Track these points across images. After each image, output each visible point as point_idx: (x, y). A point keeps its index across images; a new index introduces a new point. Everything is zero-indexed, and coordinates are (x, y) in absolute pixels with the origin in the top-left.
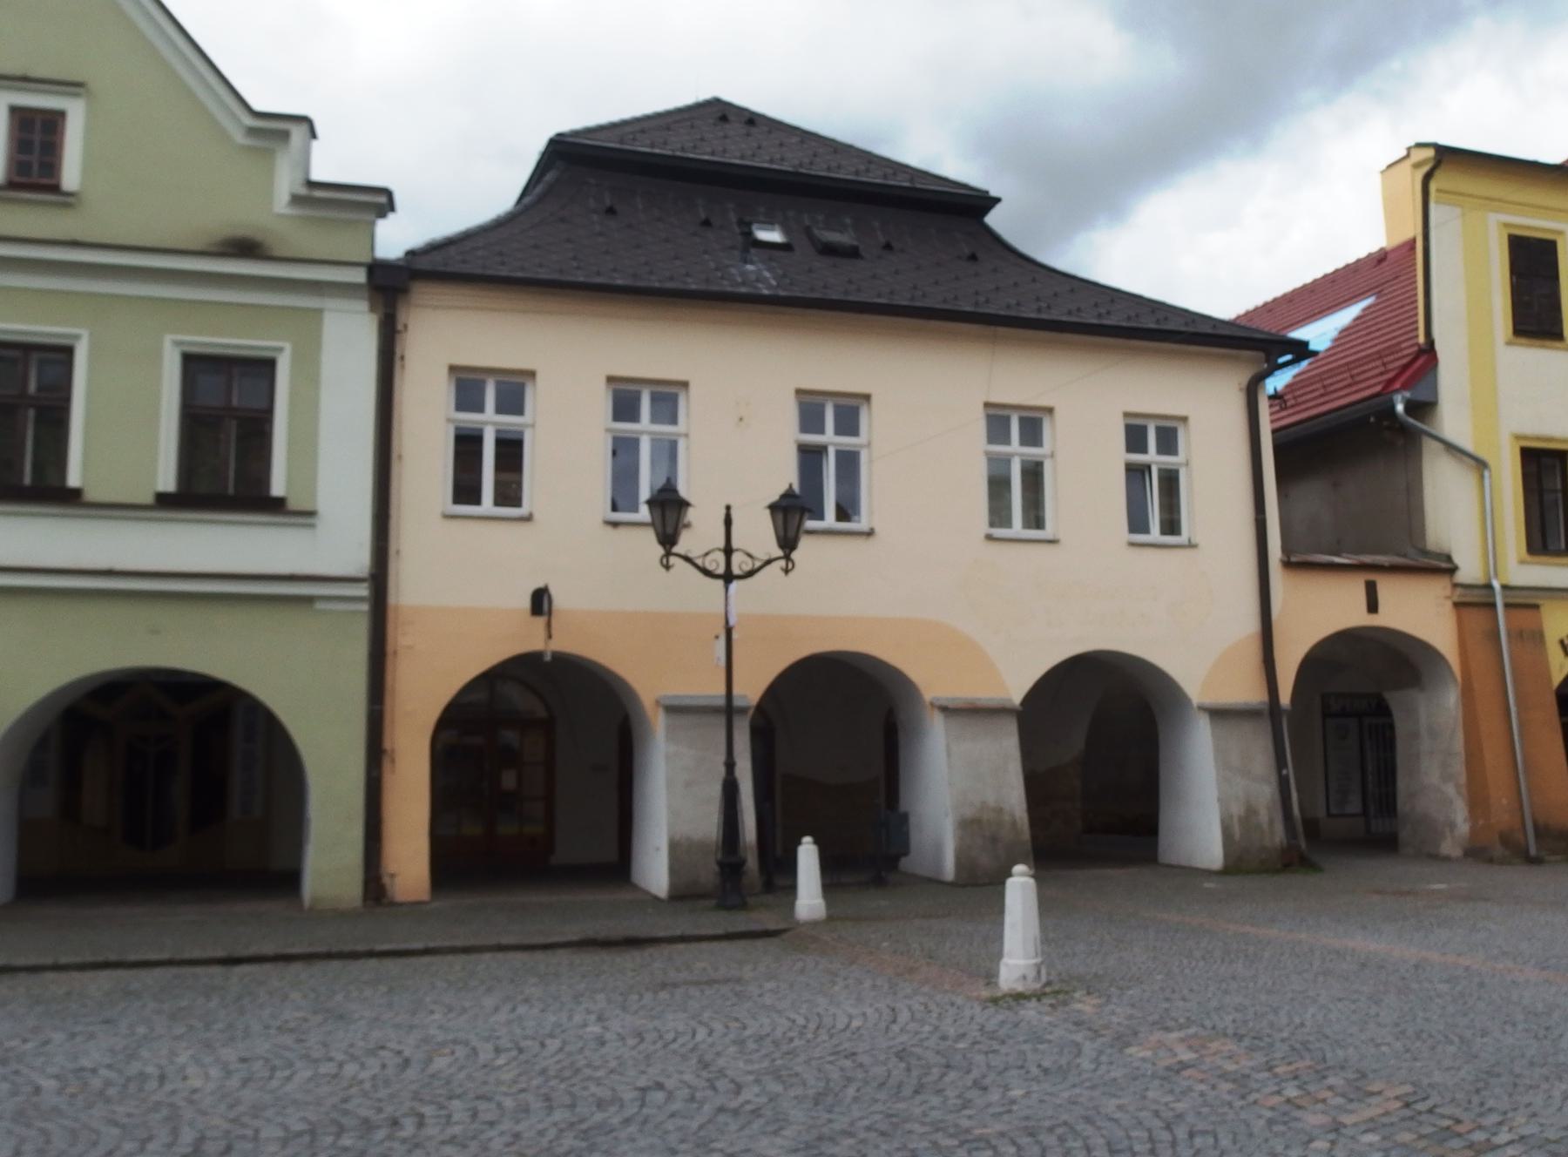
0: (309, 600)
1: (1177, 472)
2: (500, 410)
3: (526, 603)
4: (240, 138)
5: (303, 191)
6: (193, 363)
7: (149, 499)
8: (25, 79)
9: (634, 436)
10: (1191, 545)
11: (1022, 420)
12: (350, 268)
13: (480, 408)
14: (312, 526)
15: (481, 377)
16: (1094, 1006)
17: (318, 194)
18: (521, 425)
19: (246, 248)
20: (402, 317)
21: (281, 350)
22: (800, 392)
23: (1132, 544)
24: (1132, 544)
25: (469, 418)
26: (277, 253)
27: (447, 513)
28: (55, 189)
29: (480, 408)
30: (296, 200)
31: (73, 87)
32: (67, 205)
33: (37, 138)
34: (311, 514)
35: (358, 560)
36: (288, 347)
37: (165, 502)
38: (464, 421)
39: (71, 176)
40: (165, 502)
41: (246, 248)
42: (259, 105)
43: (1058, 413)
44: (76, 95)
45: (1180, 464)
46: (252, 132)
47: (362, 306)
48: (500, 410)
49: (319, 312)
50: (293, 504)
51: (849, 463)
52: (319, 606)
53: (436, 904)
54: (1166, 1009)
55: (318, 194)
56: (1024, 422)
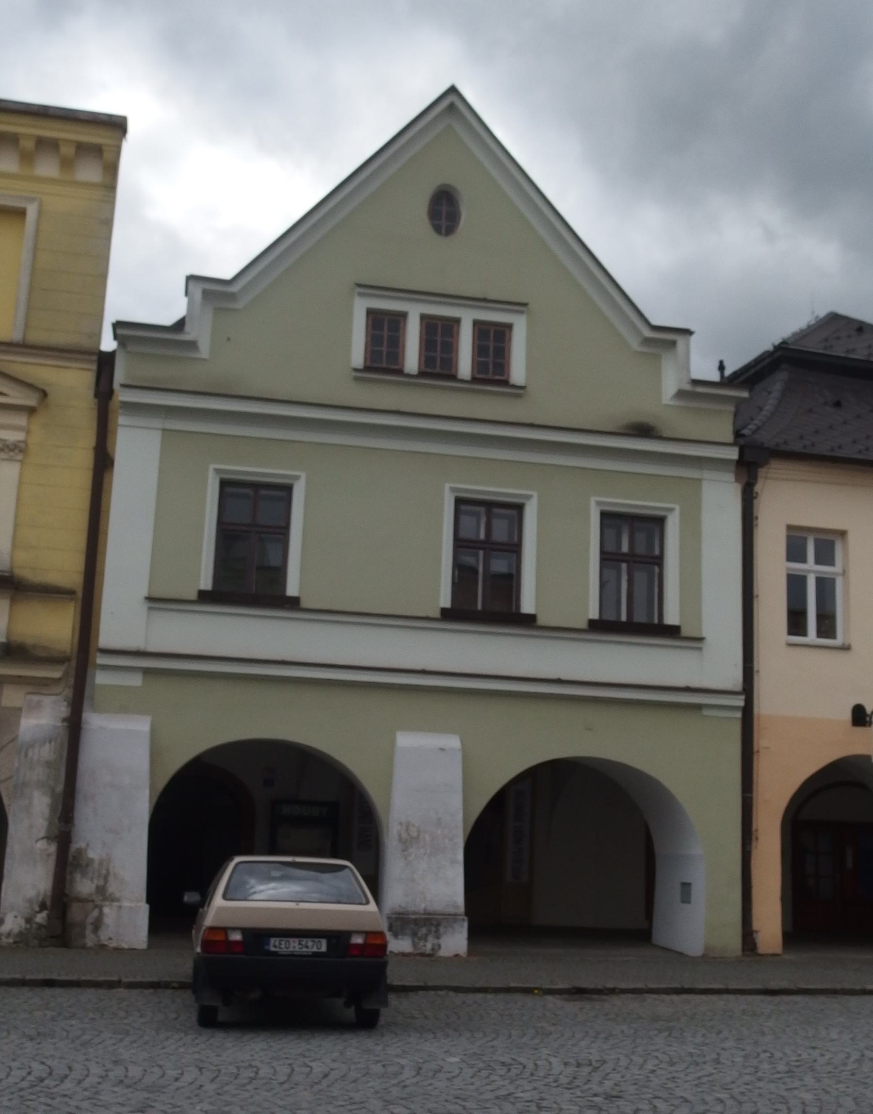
0: (699, 707)
1: (833, 581)
2: (818, 562)
3: (848, 716)
4: (635, 344)
5: (688, 387)
6: (606, 517)
7: (584, 625)
8: (485, 300)
9: (803, 574)
10: (846, 648)
11: (817, 543)
12: (175, 394)
13: (804, 560)
14: (700, 649)
15: (804, 535)
16: (742, 1056)
17: (700, 389)
18: (834, 573)
19: (644, 431)
20: (758, 488)
21: (671, 510)
22: (790, 528)
23: (790, 645)
24: (790, 645)
25: (797, 567)
26: (665, 435)
27: (789, 642)
28: (505, 383)
29: (804, 560)
30: (681, 394)
31: (520, 306)
32: (519, 396)
33: (491, 345)
34: (701, 639)
35: (733, 678)
36: (303, 475)
37: (204, 597)
38: (794, 570)
39: (518, 373)
40: (204, 597)
41: (644, 431)
42: (655, 321)
43: (851, 538)
44: (522, 312)
45: (837, 574)
46: (647, 341)
47: (730, 477)
48: (818, 562)
49: (700, 480)
50: (685, 632)
51: (825, 587)
52: (705, 712)
53: (787, 957)
54: (503, 1056)
55: (700, 389)
56: (818, 544)
